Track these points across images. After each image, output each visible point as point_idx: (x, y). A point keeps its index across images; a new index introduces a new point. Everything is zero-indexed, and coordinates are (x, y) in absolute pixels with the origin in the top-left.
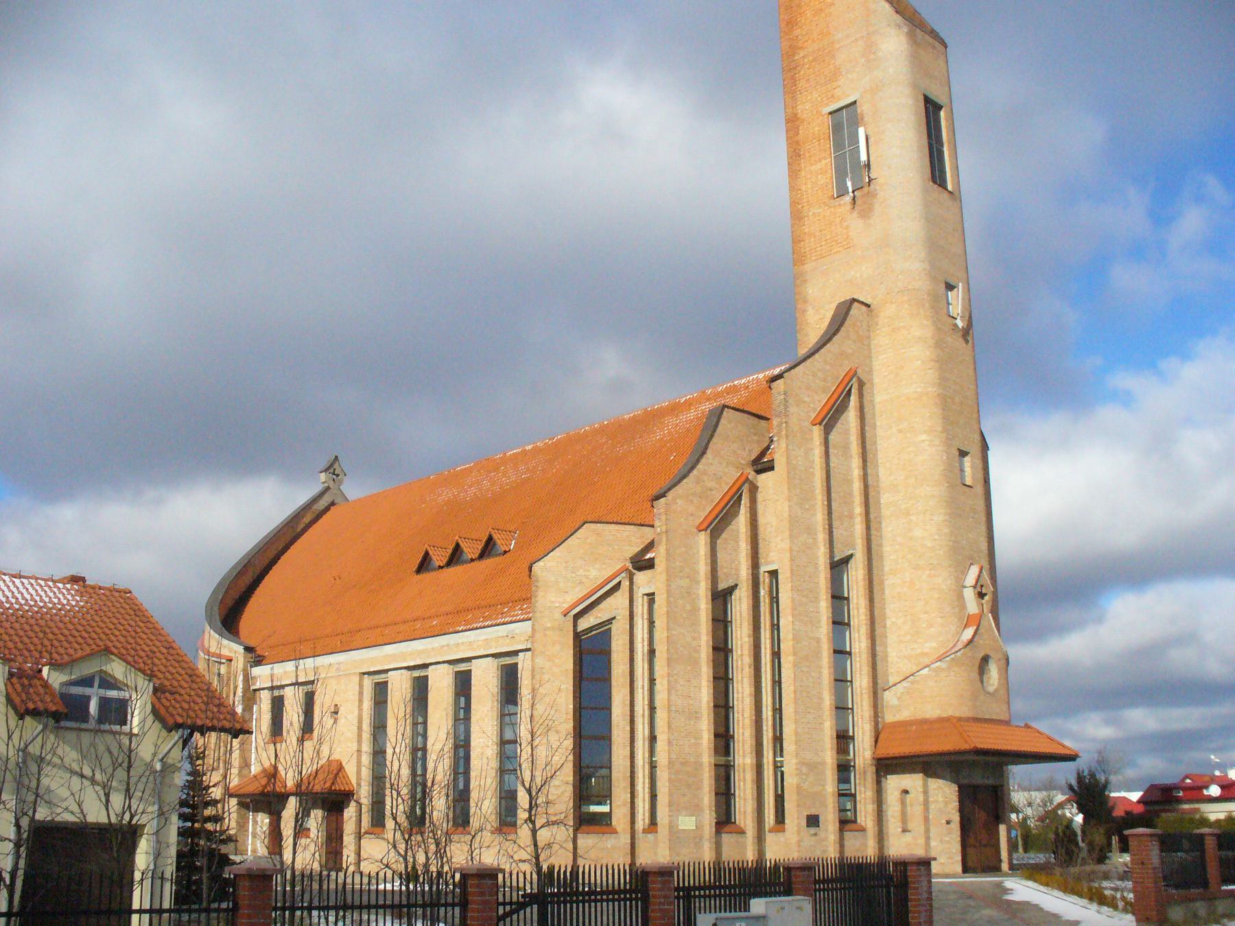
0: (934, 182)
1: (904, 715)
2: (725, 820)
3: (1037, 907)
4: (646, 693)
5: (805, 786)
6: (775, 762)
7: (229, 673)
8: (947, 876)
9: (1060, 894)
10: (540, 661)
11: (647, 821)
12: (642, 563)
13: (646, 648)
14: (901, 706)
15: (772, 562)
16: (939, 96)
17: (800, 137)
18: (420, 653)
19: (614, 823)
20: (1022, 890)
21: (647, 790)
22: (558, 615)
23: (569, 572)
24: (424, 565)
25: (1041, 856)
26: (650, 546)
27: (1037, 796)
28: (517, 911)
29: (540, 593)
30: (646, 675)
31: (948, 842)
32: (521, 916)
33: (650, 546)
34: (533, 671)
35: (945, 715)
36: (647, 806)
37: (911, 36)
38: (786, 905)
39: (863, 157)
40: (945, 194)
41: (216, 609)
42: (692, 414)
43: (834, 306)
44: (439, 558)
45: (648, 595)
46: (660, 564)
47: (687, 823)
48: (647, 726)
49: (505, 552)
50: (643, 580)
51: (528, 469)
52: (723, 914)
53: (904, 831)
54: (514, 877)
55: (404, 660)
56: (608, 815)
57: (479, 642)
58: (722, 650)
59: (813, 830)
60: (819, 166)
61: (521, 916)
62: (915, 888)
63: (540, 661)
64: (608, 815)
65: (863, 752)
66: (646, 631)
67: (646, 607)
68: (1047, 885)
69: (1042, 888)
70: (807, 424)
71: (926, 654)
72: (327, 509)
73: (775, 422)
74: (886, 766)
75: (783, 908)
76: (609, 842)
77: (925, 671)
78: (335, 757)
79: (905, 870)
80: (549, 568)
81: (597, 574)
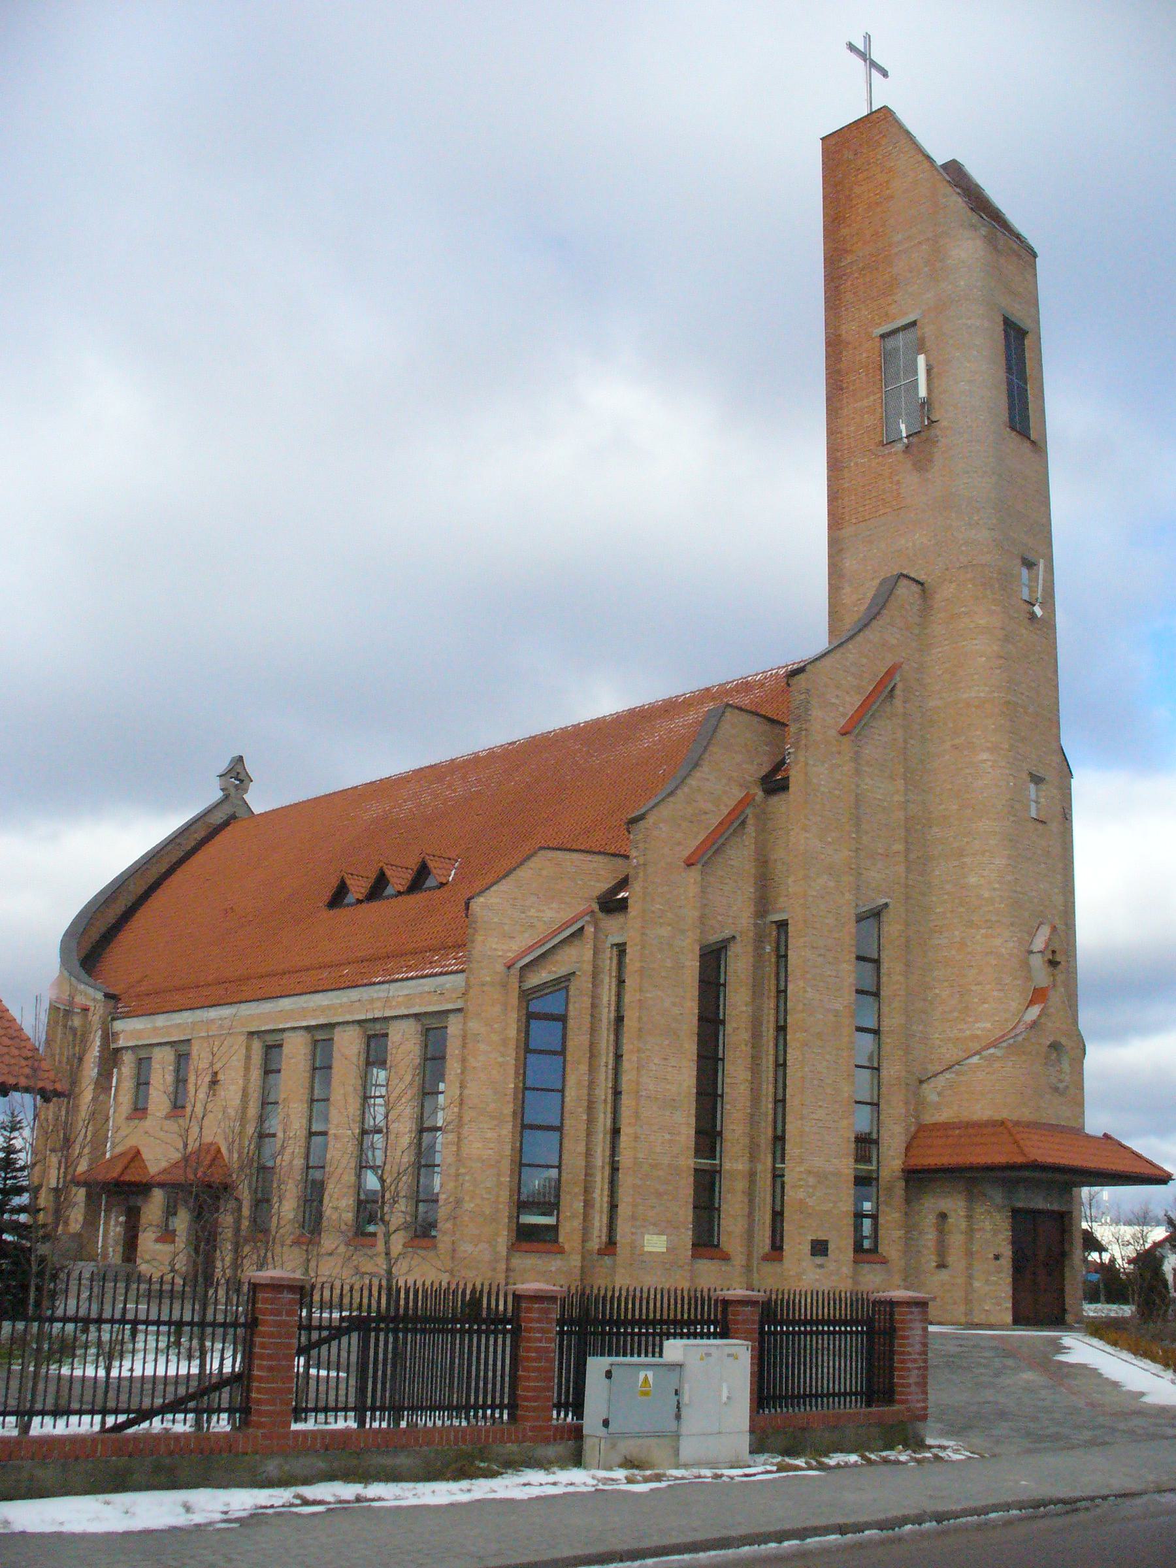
0: (1013, 428)
1: (944, 1116)
2: (706, 1242)
3: (1094, 1373)
4: (610, 1072)
5: (810, 1202)
6: (774, 1168)
7: (84, 1026)
8: (991, 1327)
9: (1128, 1356)
10: (474, 1025)
11: (604, 1239)
12: (612, 904)
13: (613, 1015)
14: (948, 1104)
15: (782, 910)
16: (1019, 315)
17: (843, 366)
18: (324, 1010)
19: (561, 1240)
20: (1082, 1350)
21: (606, 1199)
22: (500, 967)
23: (521, 910)
24: (338, 898)
25: (1126, 1308)
26: (623, 883)
27: (1127, 1232)
28: (327, 1341)
29: (479, 938)
30: (611, 1048)
31: (996, 1283)
32: (334, 1350)
33: (623, 883)
34: (464, 1037)
35: (997, 1117)
36: (605, 1220)
37: (991, 240)
38: (713, 1350)
39: (923, 392)
40: (1027, 444)
41: (74, 944)
42: (692, 716)
43: (876, 582)
44: (358, 888)
45: (618, 945)
46: (634, 909)
47: (655, 1243)
48: (609, 1116)
49: (442, 885)
50: (614, 929)
51: (479, 780)
52: (621, 1359)
53: (942, 1266)
54: (356, 1295)
55: (305, 1018)
56: (554, 1229)
57: (402, 996)
58: (710, 1023)
59: (819, 1260)
60: (865, 403)
61: (334, 1350)
62: (904, 1338)
63: (474, 1025)
64: (554, 1229)
65: (891, 1160)
66: (613, 992)
67: (615, 961)
68: (1114, 1344)
69: (1108, 1348)
70: (833, 733)
71: (977, 1037)
72: (226, 824)
73: (793, 729)
74: (918, 1178)
75: (708, 1355)
76: (554, 1264)
77: (975, 1059)
78: (207, 1139)
79: (892, 1314)
80: (492, 905)
81: (552, 915)
